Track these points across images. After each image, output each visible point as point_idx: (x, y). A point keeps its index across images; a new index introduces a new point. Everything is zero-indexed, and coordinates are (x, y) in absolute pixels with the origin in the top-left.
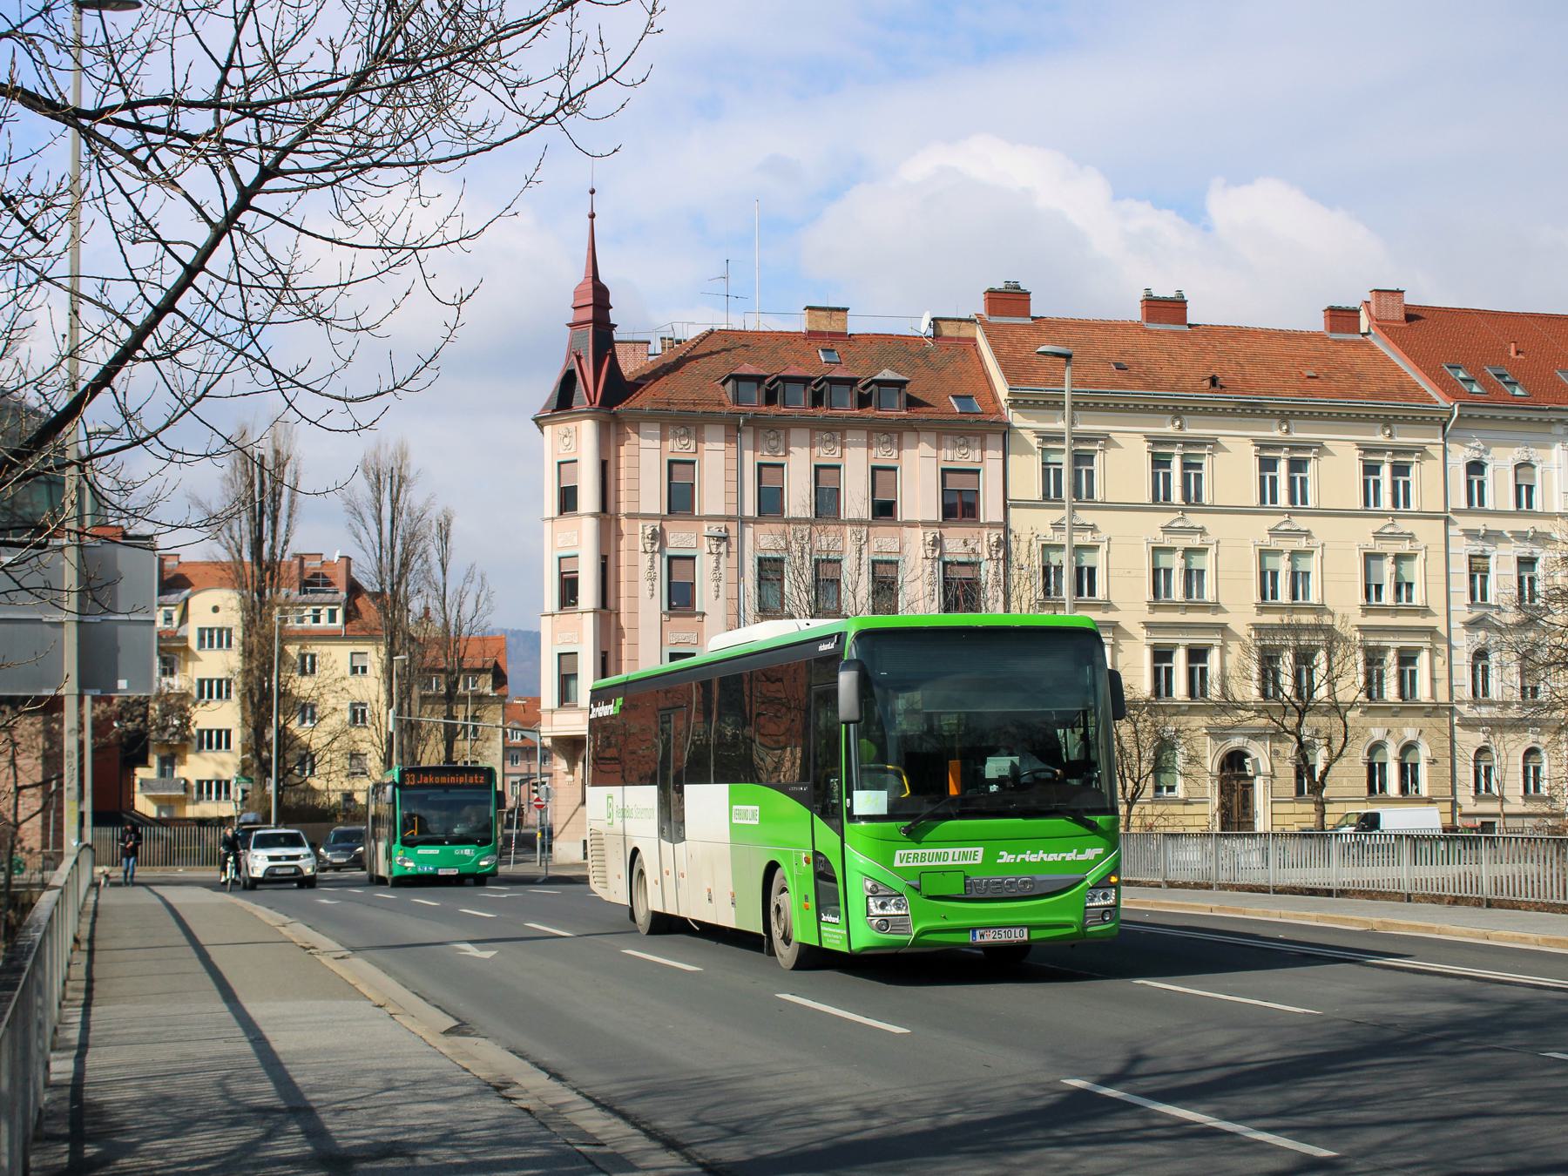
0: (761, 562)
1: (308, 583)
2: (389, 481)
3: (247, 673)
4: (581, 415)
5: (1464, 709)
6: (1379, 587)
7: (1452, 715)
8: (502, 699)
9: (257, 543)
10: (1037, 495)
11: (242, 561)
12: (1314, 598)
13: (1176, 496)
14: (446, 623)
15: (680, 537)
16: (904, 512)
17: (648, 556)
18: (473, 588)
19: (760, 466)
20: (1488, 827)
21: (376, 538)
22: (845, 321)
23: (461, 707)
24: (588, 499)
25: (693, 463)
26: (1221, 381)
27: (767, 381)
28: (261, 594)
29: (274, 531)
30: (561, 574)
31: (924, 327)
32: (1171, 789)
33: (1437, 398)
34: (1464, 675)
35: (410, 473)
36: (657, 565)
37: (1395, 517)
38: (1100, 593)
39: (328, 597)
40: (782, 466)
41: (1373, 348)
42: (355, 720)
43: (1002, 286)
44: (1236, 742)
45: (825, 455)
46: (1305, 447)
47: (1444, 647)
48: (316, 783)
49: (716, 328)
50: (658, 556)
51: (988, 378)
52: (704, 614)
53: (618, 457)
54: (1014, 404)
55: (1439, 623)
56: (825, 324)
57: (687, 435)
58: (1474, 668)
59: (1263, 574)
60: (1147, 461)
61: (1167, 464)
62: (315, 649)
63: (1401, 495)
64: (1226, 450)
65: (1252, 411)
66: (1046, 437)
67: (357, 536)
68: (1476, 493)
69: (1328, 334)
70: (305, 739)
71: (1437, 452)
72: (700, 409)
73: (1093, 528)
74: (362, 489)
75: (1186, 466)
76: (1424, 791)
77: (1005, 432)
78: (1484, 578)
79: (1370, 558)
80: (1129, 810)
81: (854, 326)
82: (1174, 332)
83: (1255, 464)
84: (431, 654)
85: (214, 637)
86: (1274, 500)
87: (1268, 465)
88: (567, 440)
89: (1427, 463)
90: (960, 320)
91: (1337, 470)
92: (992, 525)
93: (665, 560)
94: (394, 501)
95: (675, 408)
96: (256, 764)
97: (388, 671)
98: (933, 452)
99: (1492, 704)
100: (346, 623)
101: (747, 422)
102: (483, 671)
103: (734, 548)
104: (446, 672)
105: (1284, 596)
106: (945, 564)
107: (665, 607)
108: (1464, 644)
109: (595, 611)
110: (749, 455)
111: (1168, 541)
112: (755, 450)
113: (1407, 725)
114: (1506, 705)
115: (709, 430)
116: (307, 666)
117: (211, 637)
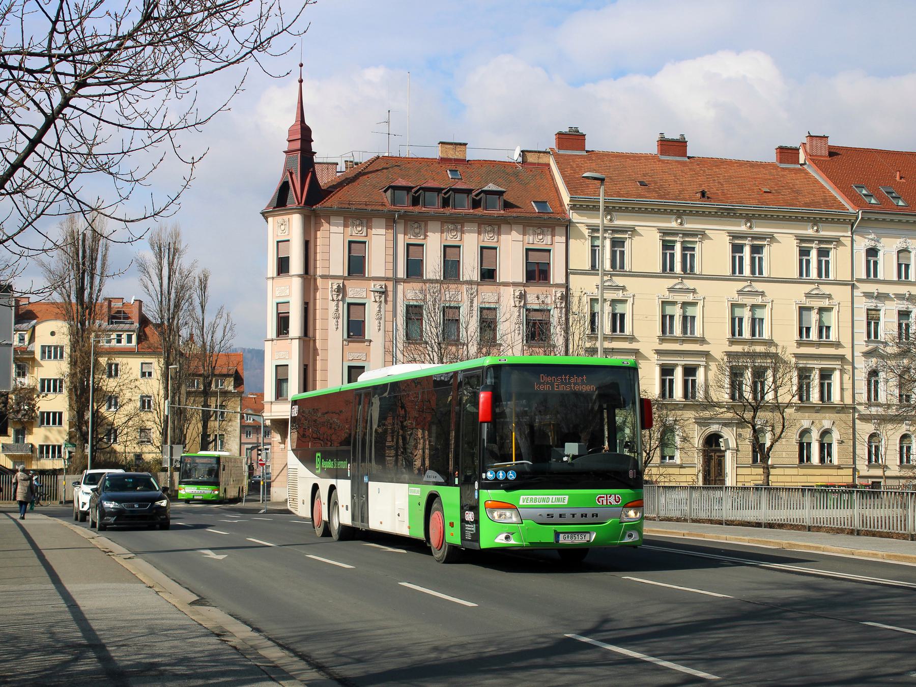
1: (114, 317)
3: (72, 375)
4: (292, 211)
6: (808, 329)
8: (240, 394)
9: (81, 291)
11: (70, 303)
12: (766, 336)
13: (678, 268)
15: (356, 291)
16: (502, 276)
17: (335, 303)
18: (222, 322)
20: (876, 485)
21: (158, 289)
24: (296, 266)
25: (365, 243)
26: (706, 195)
27: (414, 190)
28: (83, 324)
30: (278, 314)
31: (516, 156)
34: (861, 387)
35: (181, 246)
38: (628, 330)
39: (127, 327)
41: (807, 173)
43: (567, 130)
44: (714, 428)
48: (118, 448)
50: (341, 303)
52: (370, 341)
53: (316, 238)
54: (573, 207)
55: (846, 352)
56: (452, 154)
57: (361, 224)
59: (733, 320)
61: (672, 248)
62: (118, 360)
63: (824, 269)
65: (728, 214)
66: (594, 229)
69: (779, 164)
71: (847, 242)
72: (369, 208)
75: (684, 249)
76: (836, 461)
77: (568, 227)
78: (877, 324)
79: (802, 309)
81: (471, 155)
83: (729, 248)
84: (194, 364)
85: (51, 352)
86: (741, 271)
88: (283, 227)
89: (840, 248)
90: (539, 152)
94: (171, 264)
95: (353, 207)
96: (78, 435)
97: (165, 375)
101: (400, 217)
103: (390, 298)
104: (204, 380)
105: (747, 334)
108: (862, 367)
109: (299, 338)
110: (401, 237)
111: (672, 297)
113: (825, 418)
114: (889, 406)
115: (375, 221)
116: (113, 371)
117: (50, 352)
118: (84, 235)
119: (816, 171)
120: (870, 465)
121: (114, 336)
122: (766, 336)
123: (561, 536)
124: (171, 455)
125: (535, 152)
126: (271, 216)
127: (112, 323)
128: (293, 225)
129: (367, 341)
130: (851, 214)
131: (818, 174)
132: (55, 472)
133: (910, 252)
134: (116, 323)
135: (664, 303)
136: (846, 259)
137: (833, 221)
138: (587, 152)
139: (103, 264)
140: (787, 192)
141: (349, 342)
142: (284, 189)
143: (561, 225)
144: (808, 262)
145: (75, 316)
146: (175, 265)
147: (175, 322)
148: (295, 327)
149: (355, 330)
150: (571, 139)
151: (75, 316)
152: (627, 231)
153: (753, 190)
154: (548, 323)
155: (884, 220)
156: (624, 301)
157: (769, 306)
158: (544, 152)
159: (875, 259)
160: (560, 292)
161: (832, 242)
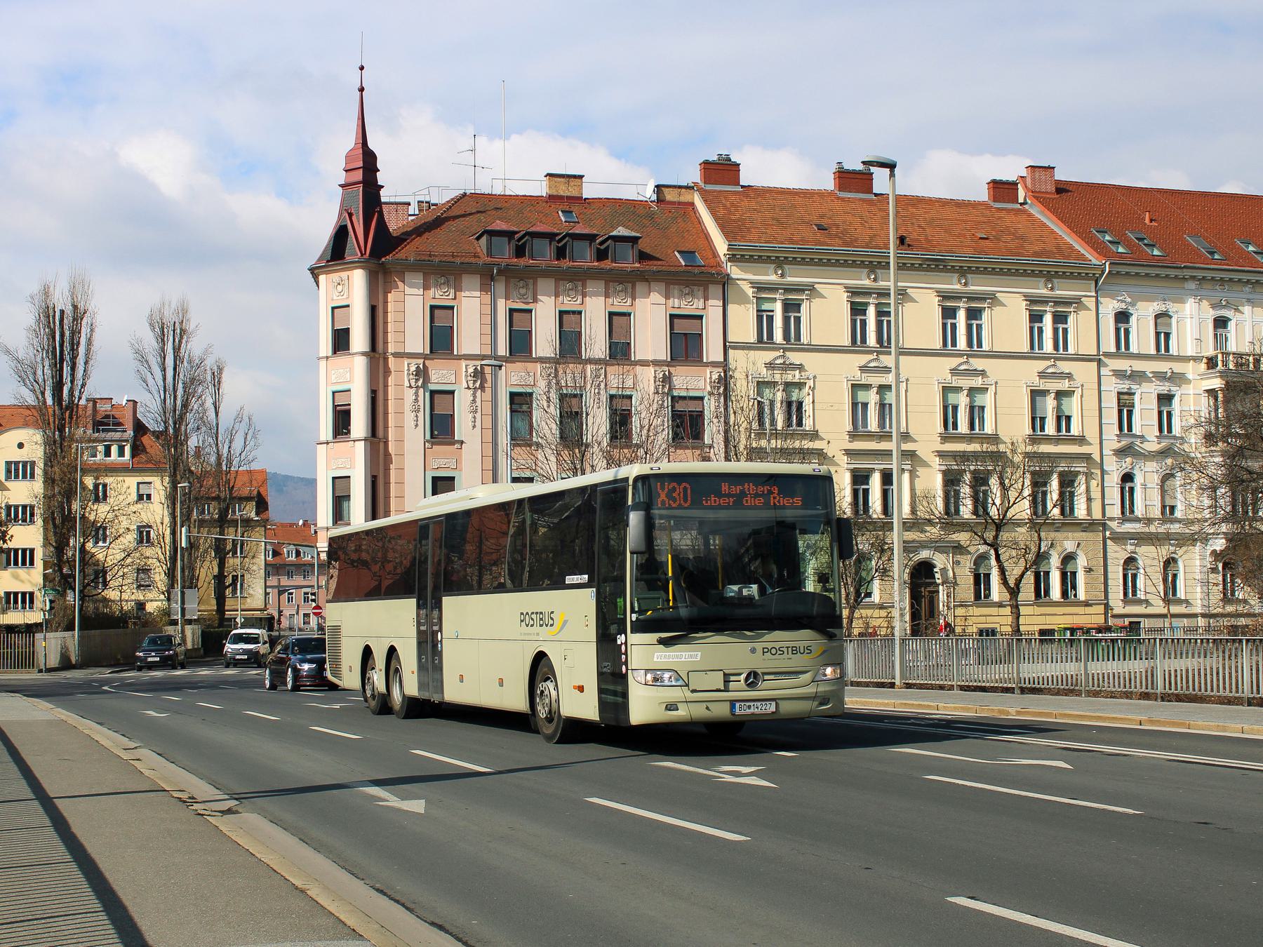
0: (513, 396)
2: (172, 334)
4: (353, 265)
5: (1114, 525)
6: (1043, 419)
7: (1104, 530)
8: (264, 523)
9: (58, 387)
10: (752, 338)
11: (45, 402)
12: (989, 429)
14: (219, 457)
15: (441, 374)
16: (639, 353)
17: (414, 390)
18: (242, 428)
19: (512, 311)
20: (1134, 627)
21: (161, 383)
22: (581, 187)
23: (232, 530)
24: (359, 340)
25: (452, 308)
26: (907, 241)
27: (517, 236)
28: (61, 430)
29: (73, 375)
30: (335, 407)
31: (649, 193)
32: (869, 595)
33: (1090, 257)
34: (1114, 495)
35: (191, 327)
36: (421, 398)
37: (1056, 359)
38: (808, 424)
39: (117, 435)
40: (530, 311)
41: (1030, 215)
42: (141, 541)
43: (715, 158)
44: (924, 554)
45: (569, 303)
46: (981, 298)
47: (1098, 472)
48: (112, 594)
49: (468, 192)
50: (421, 391)
51: (707, 237)
52: (462, 442)
53: (386, 302)
54: (733, 258)
55: (1093, 450)
56: (563, 190)
57: (447, 283)
58: (1122, 489)
59: (945, 408)
60: (846, 308)
61: (864, 312)
63: (1060, 340)
64: (913, 301)
65: (936, 266)
66: (760, 288)
67: (145, 381)
68: (1122, 337)
70: (101, 557)
71: (1090, 303)
72: (458, 261)
73: (800, 368)
74: (149, 341)
75: (881, 314)
76: (1082, 596)
77: (725, 282)
78: (1130, 413)
79: (1036, 394)
80: (852, 613)
81: (589, 191)
82: (861, 200)
83: (938, 312)
84: (209, 482)
86: (954, 344)
87: (949, 313)
88: (340, 288)
89: (1082, 313)
90: (680, 187)
91: (1007, 320)
92: (714, 364)
93: (428, 395)
94: (177, 350)
96: (58, 580)
97: (172, 498)
98: (663, 300)
99: (1138, 520)
100: (133, 456)
101: (499, 272)
102: (249, 499)
103: (488, 385)
104: (220, 503)
105: (963, 428)
106: (673, 398)
107: (428, 436)
108: (1114, 469)
109: (365, 440)
112: (507, 298)
113: (1067, 539)
114: (1149, 521)
115: (467, 280)
116: (100, 495)
117: (17, 470)
118: (62, 312)
119: (1041, 213)
120: (1126, 600)
121: (101, 448)
122: (989, 429)
123: (737, 705)
124: (183, 602)
125: (675, 187)
126: (323, 273)
127: (98, 431)
128: (353, 285)
129: (458, 442)
130: (1095, 267)
131: (1045, 215)
132: (31, 629)
133: (1171, 317)
134: (104, 430)
135: (855, 387)
136: (1085, 330)
137: (1072, 276)
138: (743, 187)
139: (88, 350)
140: (1009, 238)
141: (433, 444)
142: (340, 236)
143: (716, 283)
144: (1040, 330)
145: (51, 420)
146: (182, 350)
147: (183, 428)
148: (359, 425)
149: (441, 428)
150: (721, 171)
151: (51, 420)
152: (803, 290)
153: (964, 236)
154: (701, 414)
155: (1137, 274)
156: (800, 385)
157: (992, 389)
158: (687, 187)
159: (1126, 326)
160: (716, 373)
161: (1071, 303)
